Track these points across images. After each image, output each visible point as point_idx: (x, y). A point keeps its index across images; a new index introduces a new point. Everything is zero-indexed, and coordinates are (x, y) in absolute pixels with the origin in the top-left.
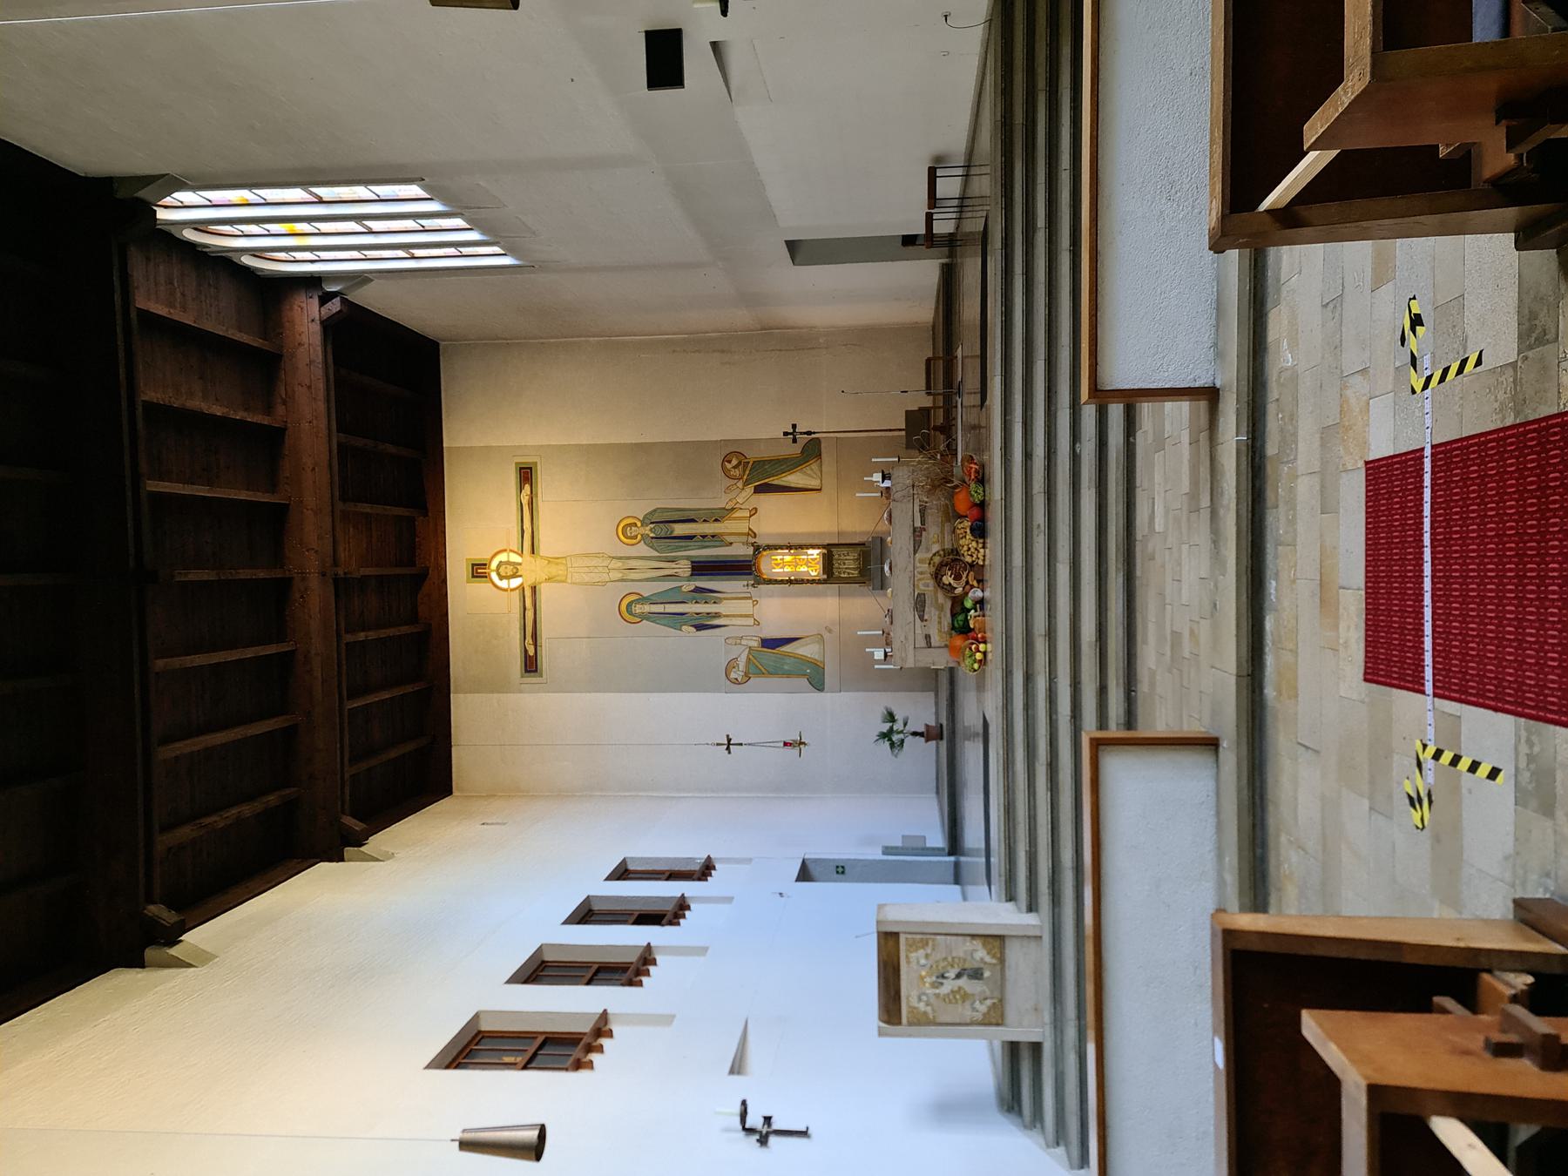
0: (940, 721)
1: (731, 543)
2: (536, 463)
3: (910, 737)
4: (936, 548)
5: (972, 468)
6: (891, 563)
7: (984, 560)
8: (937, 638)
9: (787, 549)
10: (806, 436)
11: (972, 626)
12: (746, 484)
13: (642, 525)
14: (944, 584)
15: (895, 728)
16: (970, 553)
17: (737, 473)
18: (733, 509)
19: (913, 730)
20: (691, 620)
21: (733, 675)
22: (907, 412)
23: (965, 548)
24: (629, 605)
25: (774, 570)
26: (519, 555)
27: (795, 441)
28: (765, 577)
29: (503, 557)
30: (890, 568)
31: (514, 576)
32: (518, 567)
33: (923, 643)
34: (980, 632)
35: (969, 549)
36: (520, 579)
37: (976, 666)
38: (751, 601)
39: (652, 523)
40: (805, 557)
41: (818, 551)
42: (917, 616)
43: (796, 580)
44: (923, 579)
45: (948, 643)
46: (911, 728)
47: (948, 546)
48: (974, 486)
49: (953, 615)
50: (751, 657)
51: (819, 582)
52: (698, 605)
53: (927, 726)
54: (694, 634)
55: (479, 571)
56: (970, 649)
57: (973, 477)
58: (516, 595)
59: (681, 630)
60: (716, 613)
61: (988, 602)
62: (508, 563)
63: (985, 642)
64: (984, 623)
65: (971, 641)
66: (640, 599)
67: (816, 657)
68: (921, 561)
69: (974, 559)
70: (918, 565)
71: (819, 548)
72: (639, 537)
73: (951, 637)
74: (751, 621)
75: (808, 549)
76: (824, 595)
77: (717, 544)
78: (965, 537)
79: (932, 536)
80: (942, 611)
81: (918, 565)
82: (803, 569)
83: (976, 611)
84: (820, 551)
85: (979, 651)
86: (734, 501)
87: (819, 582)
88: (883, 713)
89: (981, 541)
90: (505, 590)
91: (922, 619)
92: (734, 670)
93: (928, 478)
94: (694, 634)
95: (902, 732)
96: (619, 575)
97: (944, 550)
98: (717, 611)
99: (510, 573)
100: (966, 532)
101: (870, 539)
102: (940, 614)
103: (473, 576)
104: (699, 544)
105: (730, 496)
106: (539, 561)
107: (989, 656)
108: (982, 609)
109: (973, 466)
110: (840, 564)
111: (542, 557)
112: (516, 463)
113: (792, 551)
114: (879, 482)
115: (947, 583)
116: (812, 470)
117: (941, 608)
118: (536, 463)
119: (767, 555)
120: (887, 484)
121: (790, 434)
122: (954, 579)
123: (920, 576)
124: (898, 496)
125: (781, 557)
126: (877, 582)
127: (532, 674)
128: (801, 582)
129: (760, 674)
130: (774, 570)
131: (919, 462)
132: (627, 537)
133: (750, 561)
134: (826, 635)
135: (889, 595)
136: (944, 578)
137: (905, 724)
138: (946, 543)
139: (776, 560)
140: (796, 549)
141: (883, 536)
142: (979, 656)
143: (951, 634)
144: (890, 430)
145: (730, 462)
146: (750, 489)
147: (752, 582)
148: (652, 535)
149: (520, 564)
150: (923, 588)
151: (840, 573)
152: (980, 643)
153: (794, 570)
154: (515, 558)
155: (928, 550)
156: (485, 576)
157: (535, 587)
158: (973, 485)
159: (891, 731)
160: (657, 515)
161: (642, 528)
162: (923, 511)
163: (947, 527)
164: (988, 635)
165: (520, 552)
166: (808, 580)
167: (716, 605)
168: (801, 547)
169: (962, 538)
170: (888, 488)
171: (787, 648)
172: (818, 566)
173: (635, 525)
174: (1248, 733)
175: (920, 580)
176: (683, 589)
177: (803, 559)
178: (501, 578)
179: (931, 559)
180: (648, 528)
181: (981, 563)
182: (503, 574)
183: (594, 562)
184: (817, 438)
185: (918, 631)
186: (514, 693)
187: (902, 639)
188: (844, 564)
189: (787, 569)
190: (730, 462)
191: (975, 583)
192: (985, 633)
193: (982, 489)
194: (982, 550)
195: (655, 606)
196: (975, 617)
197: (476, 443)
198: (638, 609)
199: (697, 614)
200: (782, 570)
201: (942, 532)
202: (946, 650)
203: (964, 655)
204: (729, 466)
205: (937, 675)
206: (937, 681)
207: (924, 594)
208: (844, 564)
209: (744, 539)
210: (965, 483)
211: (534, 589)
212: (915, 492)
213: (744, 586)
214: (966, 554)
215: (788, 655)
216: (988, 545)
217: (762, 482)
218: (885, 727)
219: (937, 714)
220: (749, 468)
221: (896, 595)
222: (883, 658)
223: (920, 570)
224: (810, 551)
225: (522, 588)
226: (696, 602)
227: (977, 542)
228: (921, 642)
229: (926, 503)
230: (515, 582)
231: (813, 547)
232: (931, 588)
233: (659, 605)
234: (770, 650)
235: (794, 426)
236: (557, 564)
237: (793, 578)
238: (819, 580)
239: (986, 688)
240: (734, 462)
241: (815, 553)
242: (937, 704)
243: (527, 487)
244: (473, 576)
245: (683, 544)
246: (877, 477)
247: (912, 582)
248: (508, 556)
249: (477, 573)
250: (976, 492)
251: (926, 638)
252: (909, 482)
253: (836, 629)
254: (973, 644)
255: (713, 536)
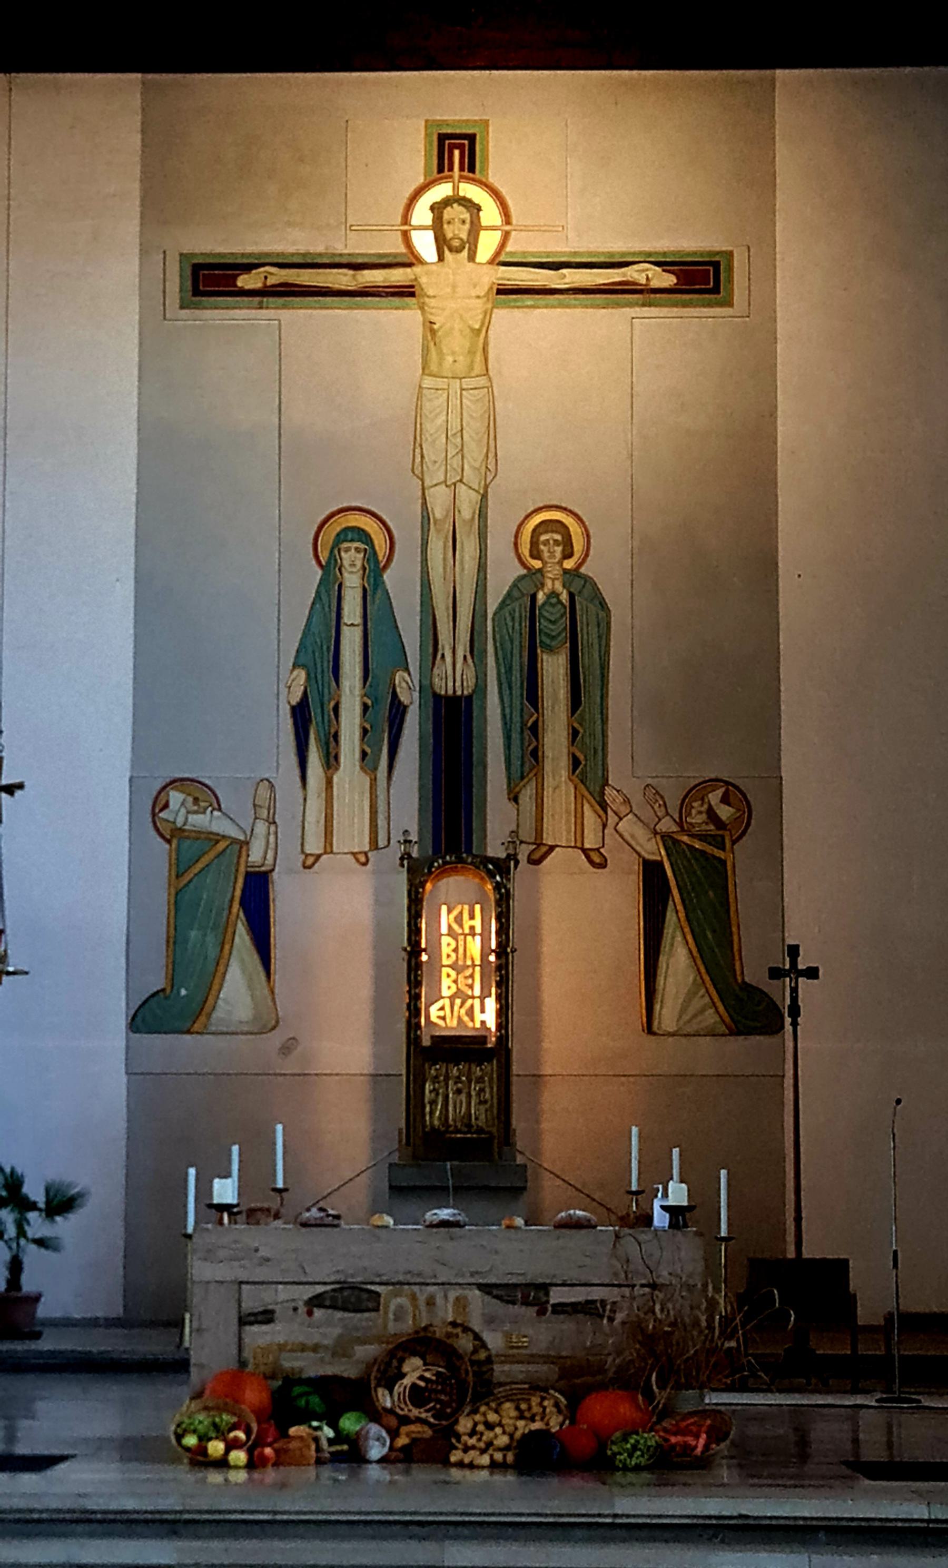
0: (47, 1332)
1: (515, 799)
2: (730, 304)
3: (7, 1256)
4: (494, 1341)
5: (697, 1437)
6: (457, 1224)
7: (460, 1465)
8: (262, 1342)
9: (499, 944)
10: (788, 1002)
11: (293, 1431)
12: (668, 840)
13: (566, 572)
14: (402, 1361)
15: (32, 1216)
16: (480, 1428)
17: (697, 818)
18: (604, 806)
19: (27, 1261)
20: (321, 695)
21: (176, 798)
22: (846, 1261)
23: (492, 1417)
24: (362, 535)
25: (444, 909)
26: (498, 253)
27: (776, 973)
28: (429, 886)
29: (490, 214)
30: (444, 1224)
31: (441, 242)
32: (465, 253)
33: (250, 1304)
34: (277, 1451)
35: (490, 1426)
36: (435, 258)
37: (191, 1441)
38: (367, 848)
39: (572, 596)
40: (477, 992)
41: (492, 1024)
42: (320, 1289)
43: (419, 965)
44: (416, 1307)
45: (250, 1368)
46: (32, 1255)
47: (500, 1370)
48: (652, 1443)
49: (323, 1385)
50: (222, 846)
51: (413, 1026)
52: (358, 709)
53: (36, 1299)
54: (283, 698)
55: (457, 153)
56: (234, 1427)
57: (673, 1440)
58: (392, 246)
59: (295, 666)
60: (337, 758)
61: (353, 1474)
62: (475, 228)
63: (251, 1465)
64: (300, 1462)
65: (255, 1427)
66: (377, 562)
67: (218, 1014)
68: (461, 1304)
69: (465, 1438)
70: (453, 1294)
71: (499, 1026)
72: (537, 564)
73: (266, 1377)
74: (314, 845)
75: (499, 998)
76: (379, 1034)
77: (516, 763)
78: (521, 1417)
79: (524, 1331)
80: (334, 1354)
81: (453, 1294)
82: (447, 987)
83: (331, 1442)
84: (493, 1029)
85: (228, 1450)
86: (623, 810)
87: (413, 1026)
88: (70, 1185)
89: (510, 1457)
90: (406, 219)
91: (315, 1302)
92: (190, 799)
93: (673, 1324)
94: (283, 698)
95: (21, 1233)
96: (438, 512)
97: (489, 1360)
98: (342, 759)
99: (449, 231)
100: (532, 1419)
101: (520, 1160)
102: (326, 1347)
103: (442, 138)
104: (517, 718)
105: (637, 799)
106: (479, 306)
107: (215, 1477)
108: (336, 1458)
109: (702, 1441)
110: (458, 1080)
111: (487, 314)
112: (730, 254)
113: (492, 958)
114: (665, 1195)
115: (406, 1368)
116: (702, 1011)
117: (341, 1350)
118: (730, 304)
119: (485, 893)
120: (660, 1219)
121: (794, 963)
122: (414, 1386)
123: (422, 1299)
124: (630, 1246)
125: (478, 930)
126: (408, 1178)
127: (189, 284)
128: (414, 981)
129: (179, 869)
130: (444, 909)
131: (712, 1305)
132: (545, 526)
133: (469, 851)
134: (276, 1039)
135: (377, 1220)
136: (417, 1361)
137: (41, 1242)
138: (506, 1367)
139: (472, 917)
140: (499, 968)
141: (525, 1197)
142: (216, 1448)
143: (273, 1377)
144: (798, 1219)
145: (725, 800)
146: (654, 850)
147: (415, 854)
148: (541, 596)
149: (472, 257)
150: (392, 1307)
151: (435, 1079)
152: (250, 1452)
153: (445, 961)
154: (488, 244)
155: (490, 1321)
156: (442, 168)
157: (412, 295)
158: (652, 1439)
159: (24, 1205)
160: (593, 609)
161: (557, 571)
162: (588, 1309)
163: (543, 1370)
164: (271, 1475)
165: (503, 258)
166: (418, 996)
167: (357, 755)
168: (503, 984)
169: (517, 1408)
170: (647, 1219)
171: (242, 936)
172: (455, 1023)
173: (568, 555)
174: (373, 1538)
175: (413, 1297)
176: (399, 676)
177: (471, 987)
178: (437, 209)
179: (466, 1329)
180: (558, 587)
181: (453, 1459)
182: (448, 213)
183: (475, 454)
184: (782, 1027)
185: (284, 1293)
186: (142, 233)
187: (263, 1253)
188: (459, 1092)
189: (447, 944)
190: (725, 800)
191: (402, 1441)
192: (276, 1464)
193: (643, 1461)
194: (485, 1460)
195: (359, 600)
196: (316, 1440)
197: (782, 150)
198: (352, 557)
199: (336, 709)
200: (444, 930)
201: (532, 1359)
202: (234, 1365)
203: (220, 1409)
204: (714, 798)
205: (168, 1324)
206: (153, 1324)
207: (377, 1309)
208: (459, 1092)
209: (527, 833)
210: (659, 1421)
211: (406, 292)
212: (638, 1291)
213: (406, 832)
214: (478, 1417)
215: (225, 941)
216: (498, 1478)
217: (673, 883)
218: (34, 1191)
219: (67, 1323)
220: (709, 849)
221: (378, 1239)
222: (216, 1200)
223: (439, 1300)
224: (491, 1004)
225: (411, 260)
226: (365, 708)
227: (506, 1448)
228: (252, 1301)
229: (611, 1320)
230: (425, 244)
231: (503, 1012)
232: (392, 1328)
233: (359, 611)
234: (238, 893)
235: (812, 973)
236: (471, 352)
237: (424, 957)
238: (418, 1025)
239: (133, 1465)
240: (725, 812)
241: (488, 1016)
242: (93, 1323)
243: (669, 280)
244: (442, 138)
245: (516, 675)
246: (678, 1194)
247: (409, 1278)
248: (493, 228)
249: (452, 148)
250: (635, 1447)
251: (266, 1312)
252: (664, 1276)
253: (290, 1066)
254: (248, 1432)
255: (535, 753)
